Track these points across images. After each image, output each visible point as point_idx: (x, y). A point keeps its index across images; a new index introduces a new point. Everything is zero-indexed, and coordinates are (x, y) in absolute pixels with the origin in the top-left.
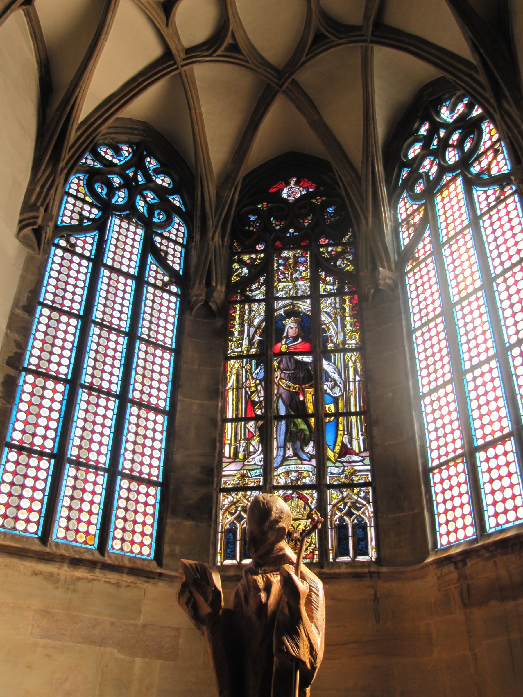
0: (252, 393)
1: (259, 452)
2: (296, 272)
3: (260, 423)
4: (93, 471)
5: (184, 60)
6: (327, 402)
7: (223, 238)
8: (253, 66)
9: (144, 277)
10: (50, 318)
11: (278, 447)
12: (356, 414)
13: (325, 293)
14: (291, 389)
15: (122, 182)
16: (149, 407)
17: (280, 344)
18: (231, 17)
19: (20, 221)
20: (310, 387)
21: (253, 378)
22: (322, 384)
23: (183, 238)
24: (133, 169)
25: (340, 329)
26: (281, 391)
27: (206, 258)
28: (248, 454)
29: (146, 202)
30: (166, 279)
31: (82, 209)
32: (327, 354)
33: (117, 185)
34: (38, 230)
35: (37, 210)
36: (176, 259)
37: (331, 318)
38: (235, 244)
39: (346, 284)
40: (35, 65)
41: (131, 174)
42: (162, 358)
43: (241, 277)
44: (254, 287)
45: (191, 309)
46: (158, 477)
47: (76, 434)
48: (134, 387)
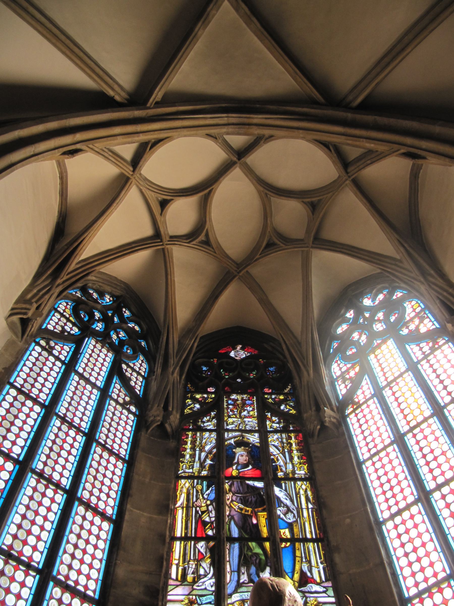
0: (203, 512)
2: (244, 411)
3: (212, 544)
4: (24, 568)
5: (168, 241)
6: (282, 527)
7: (181, 376)
8: (219, 257)
9: (109, 392)
10: (15, 399)
11: (232, 572)
12: (312, 540)
13: (271, 429)
14: (243, 512)
15: (102, 317)
16: (96, 511)
17: (231, 469)
18: (208, 219)
19: (12, 309)
20: (263, 511)
21: (204, 498)
23: (145, 372)
24: (112, 312)
25: (288, 461)
26: (233, 513)
27: (165, 388)
28: (197, 577)
29: (118, 337)
30: (127, 399)
31: (65, 324)
32: (278, 482)
33: (97, 318)
34: (26, 324)
35: (31, 304)
36: (138, 384)
37: (279, 451)
38: (189, 385)
39: (290, 424)
40: (56, 214)
41: (110, 314)
42: (115, 466)
43: (193, 410)
44: (205, 419)
45: (147, 428)
46: (94, 592)
47: (14, 521)
48: (84, 486)
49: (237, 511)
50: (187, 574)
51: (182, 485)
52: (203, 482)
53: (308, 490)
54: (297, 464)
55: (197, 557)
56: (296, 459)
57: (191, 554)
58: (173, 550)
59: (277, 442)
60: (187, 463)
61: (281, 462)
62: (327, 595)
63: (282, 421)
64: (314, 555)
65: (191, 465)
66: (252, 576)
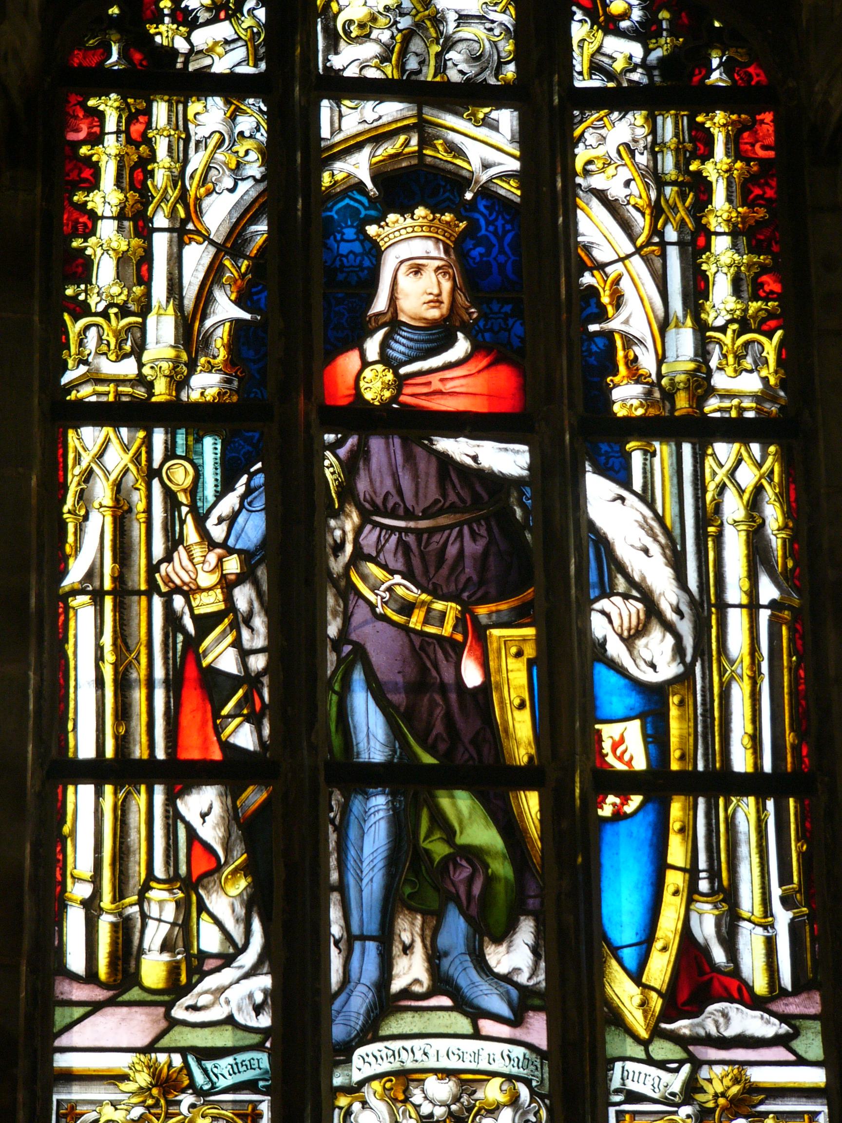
0: (207, 623)
1: (248, 959)
3: (254, 797)
12: (754, 784)
13: (596, 82)
14: (416, 621)
17: (350, 361)
21: (212, 544)
22: (585, 608)
28: (190, 967)
32: (606, 442)
49: (479, 372)
50: (141, 951)
51: (86, 459)
52: (199, 440)
53: (770, 493)
54: (723, 329)
55: (183, 870)
56: (722, 300)
57: (152, 854)
58: (66, 829)
59: (625, 173)
60: (105, 314)
61: (633, 318)
62: (792, 1058)
63: (664, 15)
64: (755, 859)
65: (129, 328)
66: (445, 963)
